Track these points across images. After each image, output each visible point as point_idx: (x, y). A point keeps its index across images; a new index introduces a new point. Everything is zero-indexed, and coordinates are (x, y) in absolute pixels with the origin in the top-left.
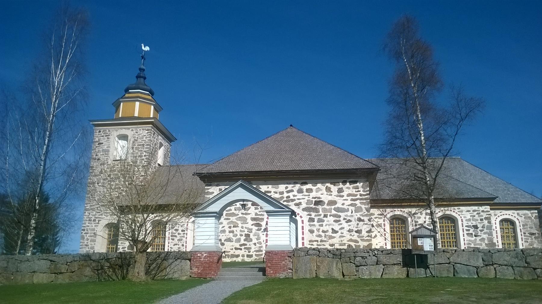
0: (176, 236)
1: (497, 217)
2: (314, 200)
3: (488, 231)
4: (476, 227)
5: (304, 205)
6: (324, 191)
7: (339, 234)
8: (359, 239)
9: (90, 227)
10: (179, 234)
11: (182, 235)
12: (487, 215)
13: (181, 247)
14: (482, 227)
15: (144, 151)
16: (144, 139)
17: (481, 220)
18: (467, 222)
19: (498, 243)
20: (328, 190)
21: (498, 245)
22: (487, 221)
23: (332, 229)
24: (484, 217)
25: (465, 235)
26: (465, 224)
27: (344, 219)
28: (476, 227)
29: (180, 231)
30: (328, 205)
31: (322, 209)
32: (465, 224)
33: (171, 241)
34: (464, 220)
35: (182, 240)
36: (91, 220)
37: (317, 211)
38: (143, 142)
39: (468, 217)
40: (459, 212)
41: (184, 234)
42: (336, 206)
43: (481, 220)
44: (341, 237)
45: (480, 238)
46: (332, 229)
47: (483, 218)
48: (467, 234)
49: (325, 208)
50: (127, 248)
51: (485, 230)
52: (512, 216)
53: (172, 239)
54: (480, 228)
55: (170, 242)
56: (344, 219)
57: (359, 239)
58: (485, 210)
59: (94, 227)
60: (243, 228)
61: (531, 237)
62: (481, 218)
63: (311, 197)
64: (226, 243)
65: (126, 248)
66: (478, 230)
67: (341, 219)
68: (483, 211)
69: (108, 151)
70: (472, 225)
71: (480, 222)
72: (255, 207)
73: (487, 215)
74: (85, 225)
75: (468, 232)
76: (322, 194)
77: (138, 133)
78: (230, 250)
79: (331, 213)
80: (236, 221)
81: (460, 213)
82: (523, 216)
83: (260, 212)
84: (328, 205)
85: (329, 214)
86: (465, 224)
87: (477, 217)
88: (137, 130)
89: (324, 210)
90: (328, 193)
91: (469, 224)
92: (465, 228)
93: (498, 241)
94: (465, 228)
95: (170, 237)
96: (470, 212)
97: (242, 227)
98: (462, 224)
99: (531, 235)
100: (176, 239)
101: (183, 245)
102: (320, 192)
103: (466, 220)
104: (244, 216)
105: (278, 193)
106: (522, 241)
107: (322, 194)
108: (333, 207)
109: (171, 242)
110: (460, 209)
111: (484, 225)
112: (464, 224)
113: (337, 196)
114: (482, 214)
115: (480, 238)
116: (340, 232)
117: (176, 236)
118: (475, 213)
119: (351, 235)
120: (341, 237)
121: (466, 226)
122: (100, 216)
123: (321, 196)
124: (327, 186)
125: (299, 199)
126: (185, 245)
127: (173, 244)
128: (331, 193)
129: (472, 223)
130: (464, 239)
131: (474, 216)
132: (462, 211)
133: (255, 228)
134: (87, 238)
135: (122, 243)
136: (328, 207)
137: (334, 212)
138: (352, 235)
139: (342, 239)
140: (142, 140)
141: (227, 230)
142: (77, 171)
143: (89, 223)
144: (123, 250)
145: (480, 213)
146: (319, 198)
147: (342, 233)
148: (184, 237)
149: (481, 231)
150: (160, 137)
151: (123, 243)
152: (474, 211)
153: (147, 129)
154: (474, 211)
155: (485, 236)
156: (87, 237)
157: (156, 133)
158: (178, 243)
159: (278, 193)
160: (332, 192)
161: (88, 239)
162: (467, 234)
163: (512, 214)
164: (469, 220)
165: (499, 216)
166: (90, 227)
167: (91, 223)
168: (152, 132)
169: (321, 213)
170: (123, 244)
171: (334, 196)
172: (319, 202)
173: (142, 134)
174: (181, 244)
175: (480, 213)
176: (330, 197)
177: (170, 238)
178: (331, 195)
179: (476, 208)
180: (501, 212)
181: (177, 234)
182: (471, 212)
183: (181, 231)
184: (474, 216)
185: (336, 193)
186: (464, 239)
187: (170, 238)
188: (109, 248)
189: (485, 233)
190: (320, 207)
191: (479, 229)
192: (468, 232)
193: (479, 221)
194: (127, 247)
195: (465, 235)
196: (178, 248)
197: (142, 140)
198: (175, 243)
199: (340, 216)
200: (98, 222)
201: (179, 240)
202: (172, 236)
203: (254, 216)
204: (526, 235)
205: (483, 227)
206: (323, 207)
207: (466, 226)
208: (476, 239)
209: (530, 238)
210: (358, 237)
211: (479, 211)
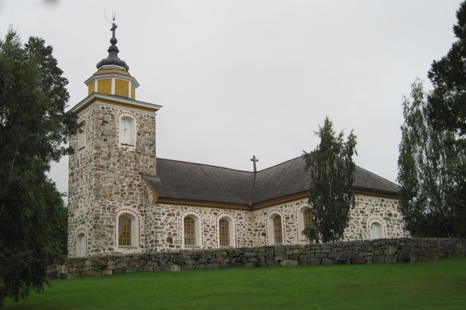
0: (208, 232)
2: (388, 212)
5: (384, 216)
10: (210, 230)
11: (213, 231)
13: (213, 242)
29: (211, 227)
33: (204, 236)
35: (213, 236)
36: (105, 208)
37: (389, 220)
41: (214, 230)
50: (166, 241)
53: (205, 234)
55: (203, 237)
59: (109, 216)
60: (358, 229)
65: (165, 240)
80: (354, 223)
83: (365, 218)
95: (203, 232)
97: (357, 229)
100: (208, 234)
101: (214, 241)
104: (357, 220)
109: (205, 237)
117: (208, 232)
125: (382, 211)
126: (216, 240)
127: (206, 239)
133: (364, 230)
135: (161, 236)
142: (335, 175)
144: (162, 242)
148: (214, 233)
158: (210, 238)
166: (105, 216)
167: (106, 212)
170: (162, 237)
172: (390, 215)
174: (212, 239)
177: (204, 233)
181: (208, 230)
183: (211, 227)
187: (204, 233)
188: (125, 240)
194: (166, 240)
196: (211, 243)
198: (208, 238)
200: (113, 210)
201: (210, 235)
202: (205, 231)
203: (362, 221)
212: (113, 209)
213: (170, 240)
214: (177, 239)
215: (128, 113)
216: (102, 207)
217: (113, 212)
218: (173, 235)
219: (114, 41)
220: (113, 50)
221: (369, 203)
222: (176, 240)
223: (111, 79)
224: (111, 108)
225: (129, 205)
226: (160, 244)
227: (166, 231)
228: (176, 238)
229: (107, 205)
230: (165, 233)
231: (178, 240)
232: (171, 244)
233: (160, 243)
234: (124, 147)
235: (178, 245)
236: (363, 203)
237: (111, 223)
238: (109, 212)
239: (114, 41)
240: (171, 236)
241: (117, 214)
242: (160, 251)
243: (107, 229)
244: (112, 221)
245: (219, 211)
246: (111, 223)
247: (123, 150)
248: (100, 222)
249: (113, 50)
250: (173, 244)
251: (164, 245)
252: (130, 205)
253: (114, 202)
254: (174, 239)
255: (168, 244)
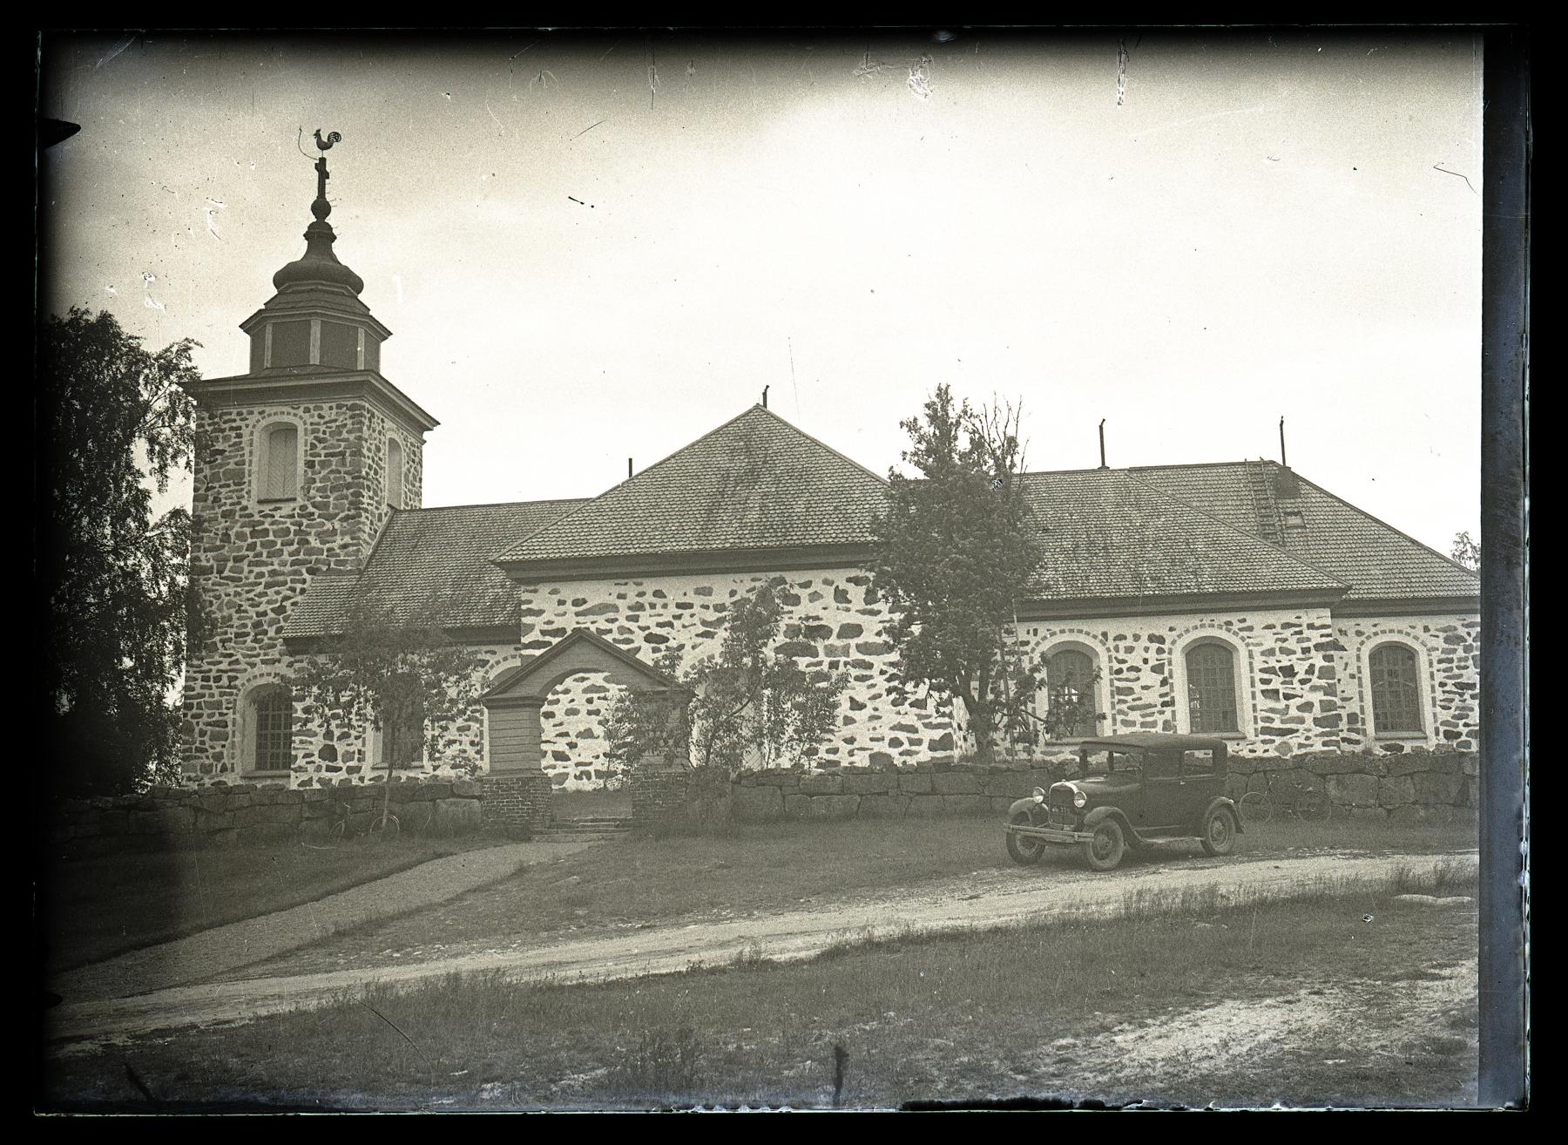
1: (1363, 638)
3: (1323, 682)
4: (1289, 672)
6: (829, 598)
7: (868, 711)
8: (919, 725)
9: (206, 699)
12: (1322, 636)
14: (1307, 672)
15: (346, 473)
16: (345, 435)
17: (1306, 650)
18: (1264, 658)
19: (1363, 713)
20: (841, 596)
21: (1363, 719)
22: (1320, 655)
23: (852, 699)
24: (1314, 642)
25: (1258, 695)
26: (1259, 662)
27: (882, 672)
28: (1289, 672)
30: (839, 636)
31: (826, 647)
32: (1258, 664)
34: (1257, 650)
38: (343, 444)
39: (1269, 642)
40: (1240, 630)
42: (860, 640)
43: (1306, 650)
44: (872, 718)
45: (1298, 701)
46: (852, 699)
47: (1310, 644)
48: (1263, 692)
49: (831, 645)
51: (1315, 681)
52: (1408, 634)
54: (1301, 676)
56: (882, 672)
57: (919, 725)
58: (1318, 623)
59: (217, 698)
61: (1461, 695)
62: (1305, 645)
63: (796, 616)
64: (581, 743)
65: (313, 755)
66: (1295, 680)
67: (875, 672)
68: (1311, 626)
69: (241, 475)
70: (1278, 666)
71: (1303, 656)
72: (653, 645)
73: (1322, 636)
74: (192, 693)
75: (1265, 687)
76: (825, 609)
77: (327, 419)
78: (593, 760)
79: (848, 656)
81: (1245, 634)
82: (1442, 635)
84: (839, 636)
85: (843, 659)
86: (1258, 664)
87: (1292, 644)
88: (322, 409)
89: (830, 651)
90: (840, 605)
91: (1270, 665)
92: (1258, 676)
93: (1362, 708)
94: (1258, 676)
96: (1274, 631)
98: (1251, 664)
99: (1462, 689)
102: (819, 604)
103: (1263, 653)
105: (711, 607)
106: (1434, 705)
107: (825, 609)
108: (853, 642)
110: (1244, 620)
111: (1312, 666)
112: (1254, 665)
113: (864, 612)
114: (1307, 633)
115: (1298, 701)
116: (870, 705)
118: (1287, 633)
119: (899, 713)
120: (872, 718)
121: (1260, 670)
122: (233, 667)
123: (821, 613)
124: (837, 587)
128: (849, 606)
129: (1279, 661)
130: (1254, 706)
131: (1285, 640)
132: (1250, 629)
134: (201, 729)
135: (302, 742)
136: (839, 643)
137: (855, 655)
138: (902, 712)
139: (875, 723)
140: (338, 440)
141: (584, 708)
143: (202, 687)
145: (1301, 633)
146: (817, 618)
147: (876, 709)
149: (1303, 682)
150: (388, 424)
151: (306, 742)
152: (1286, 626)
153: (349, 403)
154: (1286, 626)
155: (1317, 698)
156: (201, 725)
157: (376, 413)
158: (459, 738)
159: (711, 607)
160: (850, 602)
161: (202, 733)
162: (1263, 692)
163: (1409, 630)
164: (1271, 652)
165: (1369, 637)
166: (206, 699)
168: (365, 413)
169: (822, 656)
171: (857, 611)
173: (336, 421)
175: (1301, 633)
176: (844, 614)
178: (848, 610)
179: (1289, 616)
180: (1375, 625)
182: (1278, 629)
184: (1285, 640)
185: (862, 606)
186: (1254, 706)
189: (1314, 689)
190: (820, 645)
191: (1298, 677)
192: (1265, 687)
193: (1299, 655)
195: (1258, 695)
197: (338, 440)
199: (870, 666)
204: (1446, 689)
205: (1310, 670)
206: (827, 642)
207: (1260, 670)
208: (1287, 706)
209: (1457, 698)
210: (920, 717)
211: (1300, 626)
212: (229, 677)
213: (329, 753)
214: (351, 749)
215: (283, 413)
216: (199, 676)
217: (229, 687)
218: (339, 739)
219: (321, 208)
220: (320, 236)
221: (698, 601)
222: (347, 752)
223: (309, 321)
224: (235, 411)
225: (274, 661)
226: (300, 767)
227: (318, 730)
228: (348, 745)
229: (214, 668)
230: (315, 734)
231: (354, 752)
232: (330, 764)
233: (301, 762)
234: (267, 509)
235: (351, 764)
236: (665, 606)
237: (221, 714)
238: (218, 687)
239: (321, 208)
240: (332, 740)
241: (239, 690)
242: (299, 785)
243: (212, 732)
244: (225, 711)
245: (494, 653)
246: (221, 714)
247: (265, 516)
248: (193, 717)
249: (320, 236)
250: (339, 763)
251: (311, 768)
252: (279, 661)
253: (234, 658)
254: (341, 748)
255: (324, 764)
